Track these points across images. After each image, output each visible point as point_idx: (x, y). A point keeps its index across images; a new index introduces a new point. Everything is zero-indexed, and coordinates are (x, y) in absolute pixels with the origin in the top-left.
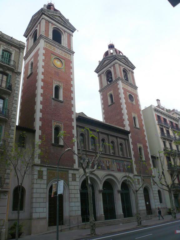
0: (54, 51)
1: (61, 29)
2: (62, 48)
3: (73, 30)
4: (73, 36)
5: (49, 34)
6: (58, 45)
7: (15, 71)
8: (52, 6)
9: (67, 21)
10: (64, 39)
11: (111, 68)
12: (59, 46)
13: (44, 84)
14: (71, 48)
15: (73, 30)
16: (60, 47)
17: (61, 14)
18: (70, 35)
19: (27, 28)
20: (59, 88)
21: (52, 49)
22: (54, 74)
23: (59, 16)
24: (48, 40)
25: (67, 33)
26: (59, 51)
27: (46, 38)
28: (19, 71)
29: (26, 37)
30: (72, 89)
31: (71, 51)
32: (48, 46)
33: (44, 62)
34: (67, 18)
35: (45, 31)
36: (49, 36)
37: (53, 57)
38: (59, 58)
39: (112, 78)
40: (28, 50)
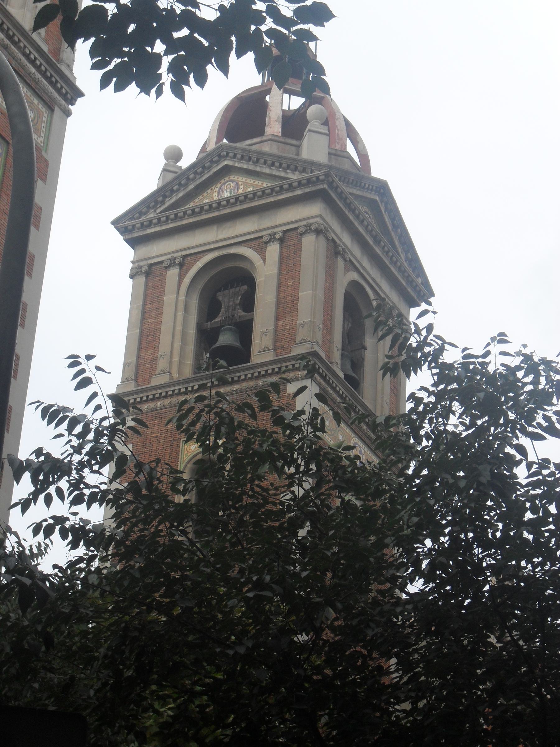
1: (368, 289)
11: (262, 252)
39: (245, 330)
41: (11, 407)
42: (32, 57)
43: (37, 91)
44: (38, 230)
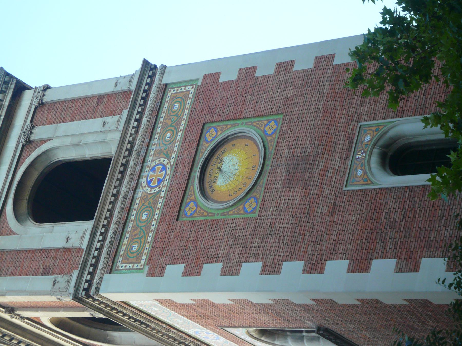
0: (160, 203)
2: (130, 151)
4: (46, 88)
5: (60, 243)
6: (120, 181)
10: (77, 145)
12: (123, 173)
13: (384, 256)
14: (123, 87)
16: (125, 165)
18: (42, 104)
20: (394, 140)
21: (147, 218)
22: (305, 187)
24: (99, 250)
25: (36, 130)
27: (86, 270)
30: (304, 64)
32: (135, 248)
33: (240, 264)
35: (46, 272)
36: (75, 242)
37: (197, 206)
38: (200, 167)
42: (136, 124)
43: (119, 238)
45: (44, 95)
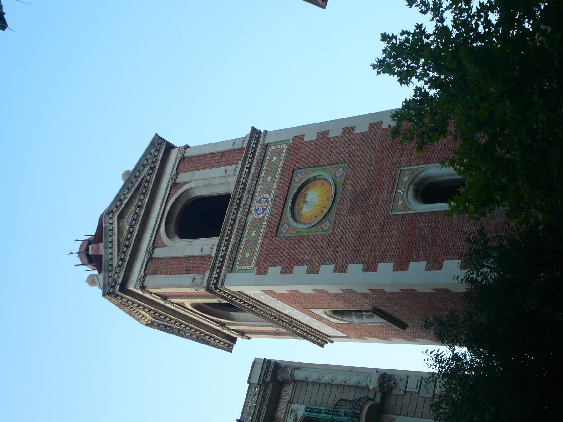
2: (243, 189)
3: (160, 148)
4: (187, 147)
5: (197, 253)
6: (237, 210)
7: (378, 399)
8: (87, 249)
9: (130, 178)
10: (207, 186)
12: (239, 204)
13: (418, 259)
15: (160, 148)
16: (240, 199)
17: (109, 212)
18: (183, 158)
19: (198, 339)
20: (424, 180)
23: (121, 217)
24: (224, 257)
25: (180, 176)
26: (259, 202)
28: (373, 384)
29: (234, 340)
30: (310, 137)
31: (249, 145)
32: (248, 255)
33: (319, 266)
34: (122, 183)
35: (188, 272)
36: (206, 252)
37: (289, 227)
38: (290, 199)
40: (283, 330)
41: (123, 178)
42: (247, 171)
44: (354, 127)
45: (185, 152)
